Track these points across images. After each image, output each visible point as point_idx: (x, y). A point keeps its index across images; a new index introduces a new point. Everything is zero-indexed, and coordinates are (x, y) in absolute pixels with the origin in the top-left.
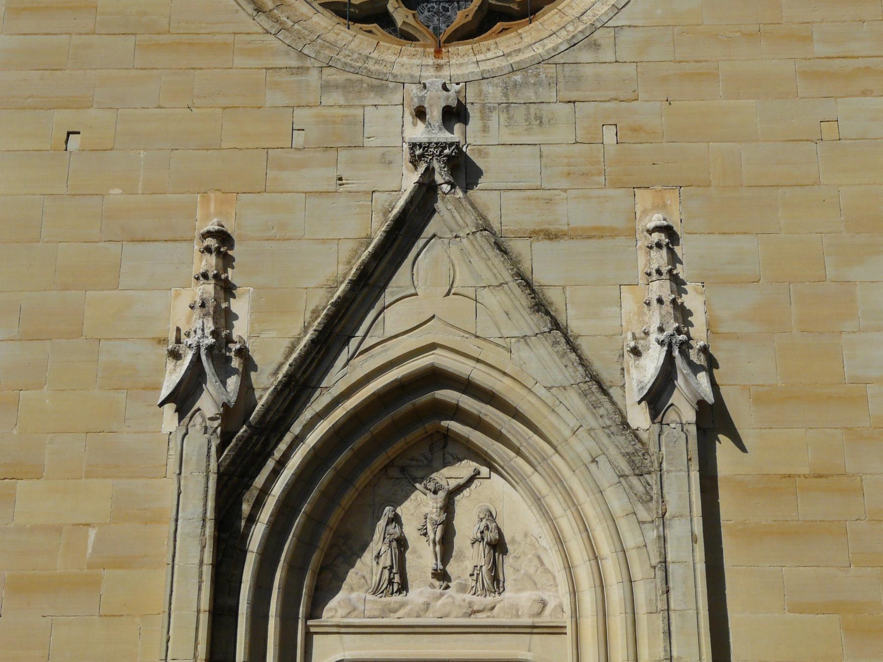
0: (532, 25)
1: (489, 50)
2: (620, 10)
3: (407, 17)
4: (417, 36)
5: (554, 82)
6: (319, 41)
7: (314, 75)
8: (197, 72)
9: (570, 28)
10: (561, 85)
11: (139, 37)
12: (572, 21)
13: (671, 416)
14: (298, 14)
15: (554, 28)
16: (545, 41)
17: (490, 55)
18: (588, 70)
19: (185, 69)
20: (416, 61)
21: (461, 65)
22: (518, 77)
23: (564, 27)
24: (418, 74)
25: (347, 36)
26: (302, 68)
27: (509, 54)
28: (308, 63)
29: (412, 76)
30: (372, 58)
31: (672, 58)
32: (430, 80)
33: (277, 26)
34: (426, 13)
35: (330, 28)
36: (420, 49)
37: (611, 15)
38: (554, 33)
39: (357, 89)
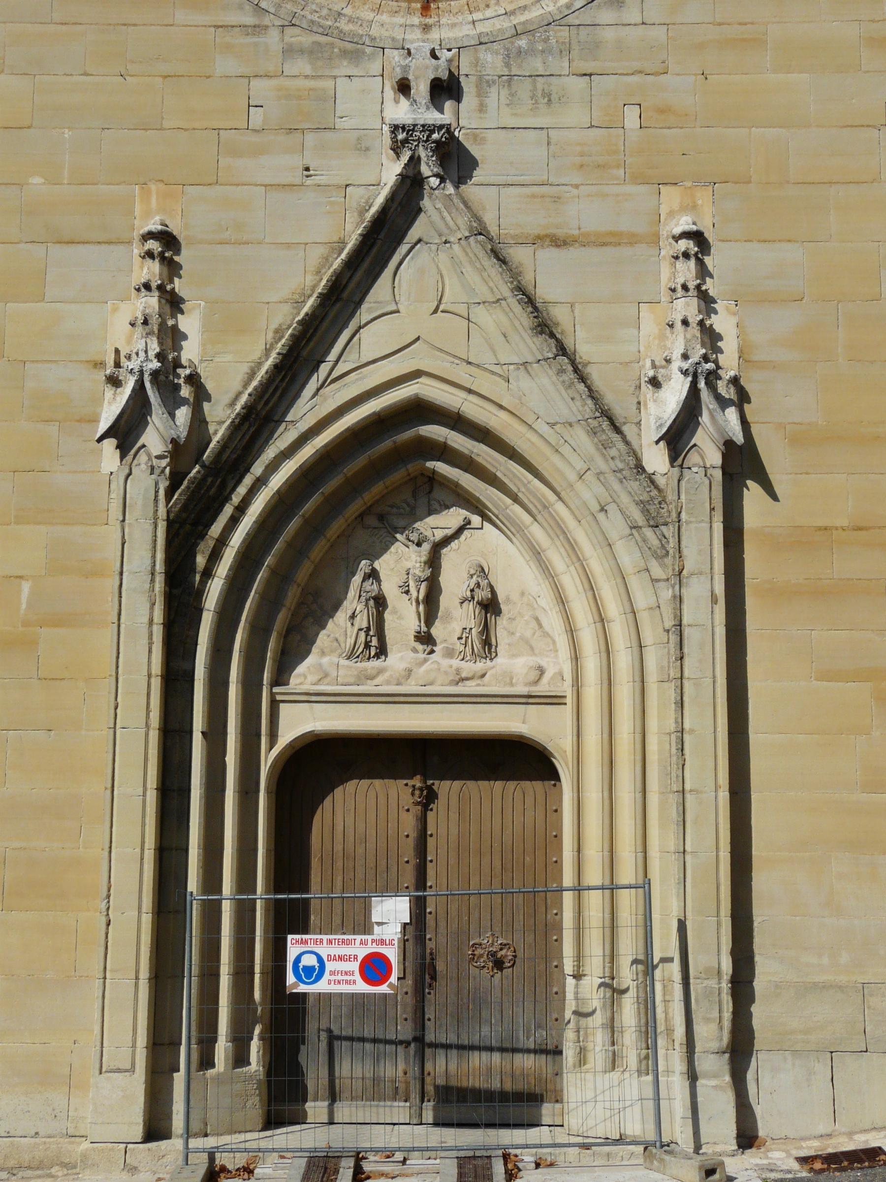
5: (566, 50)
7: (273, 36)
10: (575, 53)
13: (693, 458)
18: (609, 34)
19: (114, 25)
20: (399, 20)
21: (454, 25)
22: (523, 42)
24: (400, 37)
26: (259, 26)
27: (513, 13)
28: (267, 20)
29: (393, 39)
30: (345, 15)
39: (326, 55)
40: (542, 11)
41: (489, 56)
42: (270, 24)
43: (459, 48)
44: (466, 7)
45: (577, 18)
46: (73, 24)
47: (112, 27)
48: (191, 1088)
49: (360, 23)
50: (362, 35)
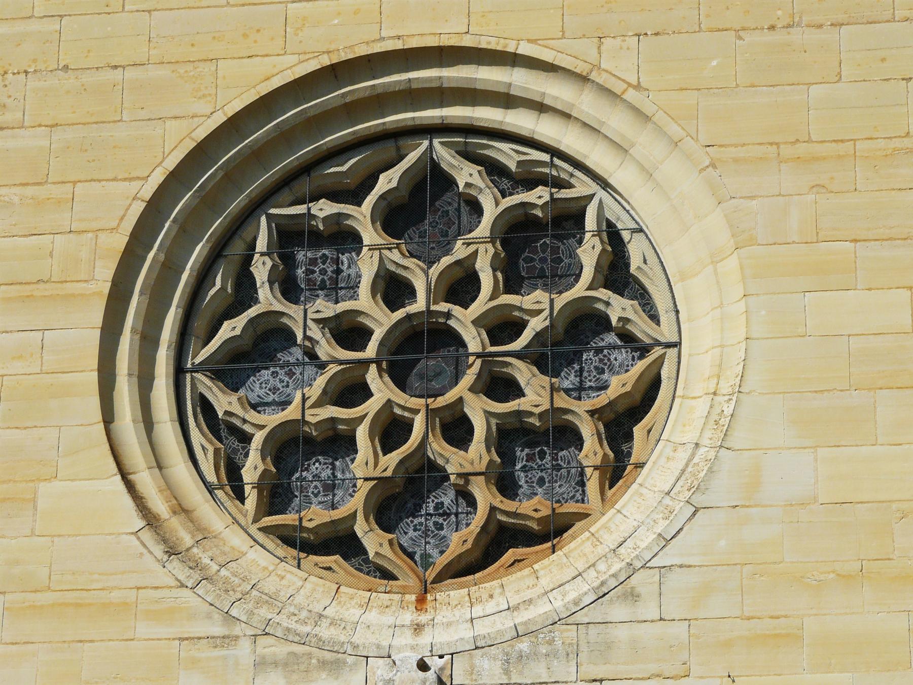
0: (559, 553)
1: (491, 596)
2: (668, 541)
3: (381, 545)
4: (395, 572)
6: (254, 593)
7: (245, 645)
8: (87, 645)
9: (602, 566)
10: (583, 657)
11: (9, 597)
12: (605, 556)
14: (226, 549)
15: (581, 566)
16: (567, 586)
17: (491, 607)
18: (621, 633)
19: (69, 642)
20: (388, 619)
21: (449, 624)
22: (524, 645)
23: (594, 565)
24: (385, 644)
25: (295, 579)
26: (228, 637)
27: (517, 608)
28: (237, 630)
29: (378, 646)
30: (326, 617)
31: (738, 613)
32: (401, 655)
33: (197, 576)
34: (411, 533)
35: (271, 568)
36: (397, 597)
37: (656, 549)
38: (580, 574)
39: (302, 667)
40: (548, 607)
41: (486, 662)
42: (241, 634)
43: (452, 654)
44: (467, 598)
45: (586, 615)
46: (25, 643)
47: (66, 645)
48: (111, 460)
49: (343, 626)
50: (343, 643)
